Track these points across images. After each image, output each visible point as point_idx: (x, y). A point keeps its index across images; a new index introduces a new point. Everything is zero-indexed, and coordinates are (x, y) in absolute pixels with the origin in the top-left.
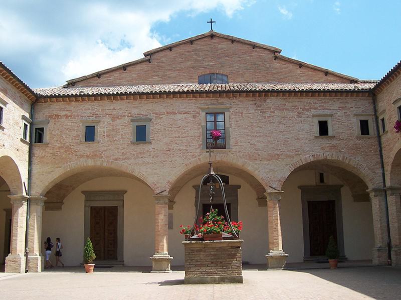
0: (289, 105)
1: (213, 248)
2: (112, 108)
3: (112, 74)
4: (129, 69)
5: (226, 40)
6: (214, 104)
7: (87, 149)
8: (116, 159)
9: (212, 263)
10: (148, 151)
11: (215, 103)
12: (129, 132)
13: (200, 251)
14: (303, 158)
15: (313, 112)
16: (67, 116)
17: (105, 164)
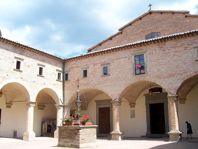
0: (179, 44)
1: (69, 129)
2: (93, 60)
3: (106, 43)
4: (113, 39)
5: (159, 13)
6: (138, 51)
7: (83, 81)
8: (96, 85)
9: (68, 137)
10: (109, 79)
11: (139, 50)
12: (100, 71)
13: (63, 131)
14: (188, 74)
15: (194, 45)
16: (76, 67)
17: (91, 88)
